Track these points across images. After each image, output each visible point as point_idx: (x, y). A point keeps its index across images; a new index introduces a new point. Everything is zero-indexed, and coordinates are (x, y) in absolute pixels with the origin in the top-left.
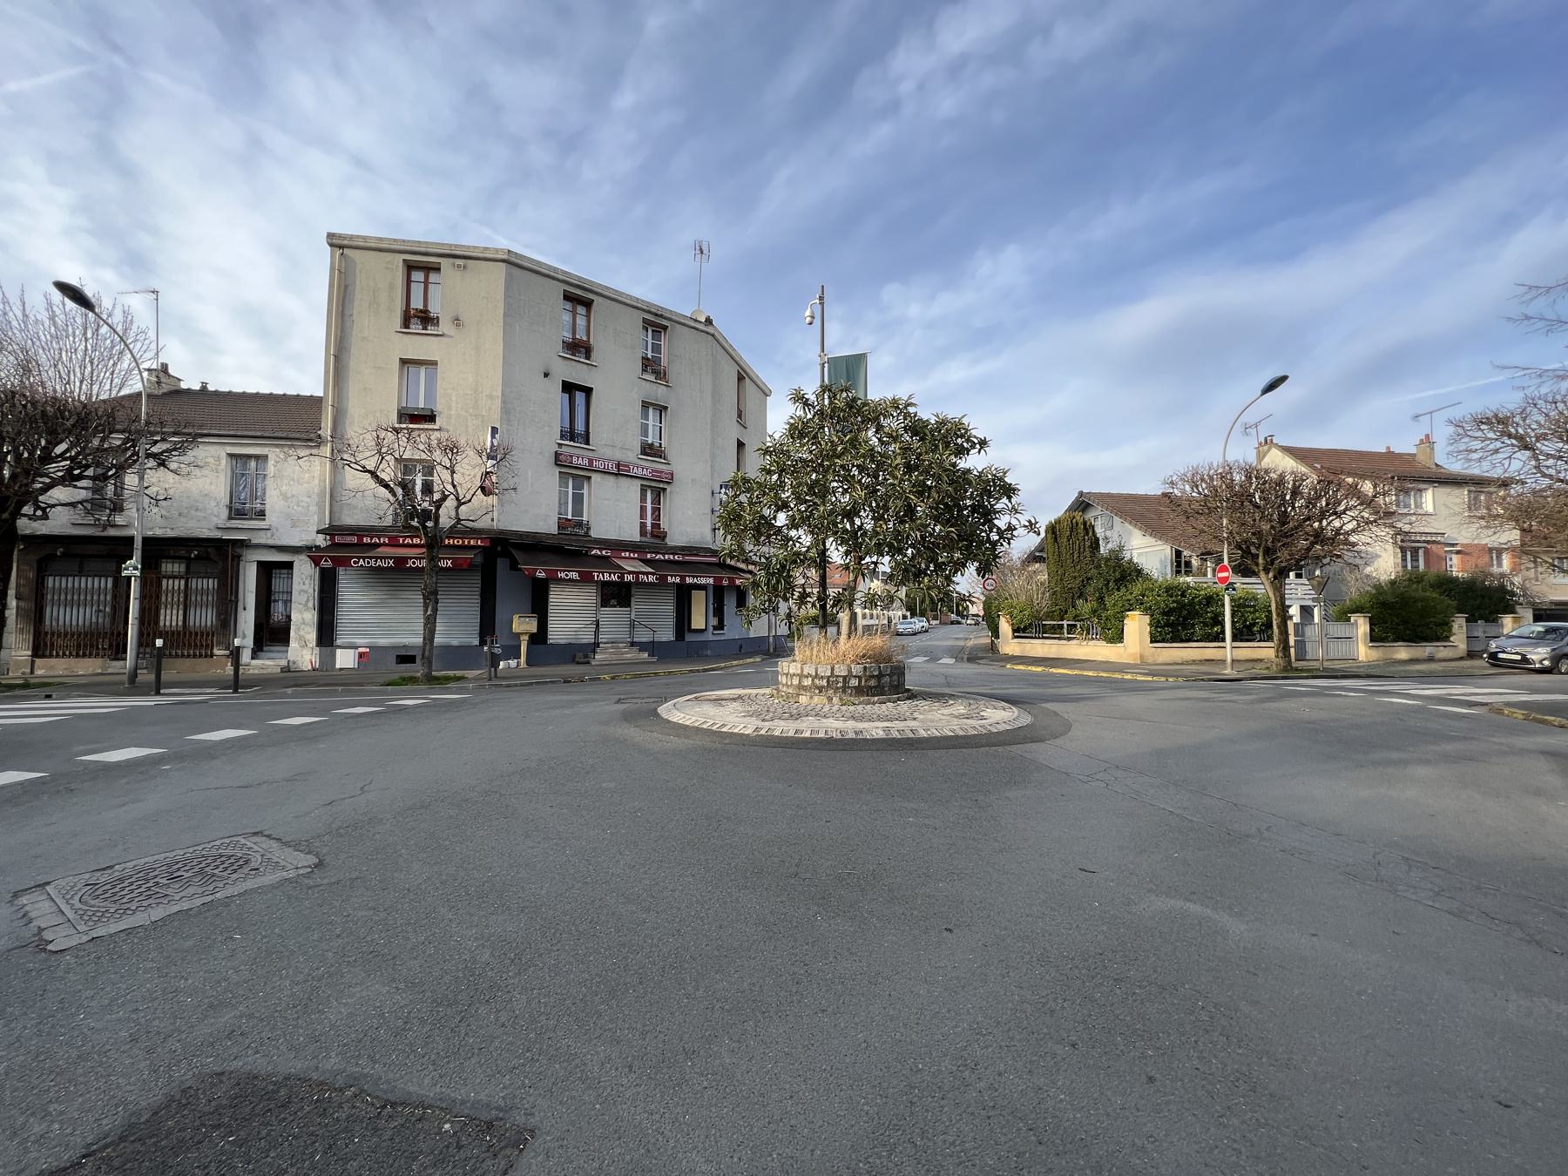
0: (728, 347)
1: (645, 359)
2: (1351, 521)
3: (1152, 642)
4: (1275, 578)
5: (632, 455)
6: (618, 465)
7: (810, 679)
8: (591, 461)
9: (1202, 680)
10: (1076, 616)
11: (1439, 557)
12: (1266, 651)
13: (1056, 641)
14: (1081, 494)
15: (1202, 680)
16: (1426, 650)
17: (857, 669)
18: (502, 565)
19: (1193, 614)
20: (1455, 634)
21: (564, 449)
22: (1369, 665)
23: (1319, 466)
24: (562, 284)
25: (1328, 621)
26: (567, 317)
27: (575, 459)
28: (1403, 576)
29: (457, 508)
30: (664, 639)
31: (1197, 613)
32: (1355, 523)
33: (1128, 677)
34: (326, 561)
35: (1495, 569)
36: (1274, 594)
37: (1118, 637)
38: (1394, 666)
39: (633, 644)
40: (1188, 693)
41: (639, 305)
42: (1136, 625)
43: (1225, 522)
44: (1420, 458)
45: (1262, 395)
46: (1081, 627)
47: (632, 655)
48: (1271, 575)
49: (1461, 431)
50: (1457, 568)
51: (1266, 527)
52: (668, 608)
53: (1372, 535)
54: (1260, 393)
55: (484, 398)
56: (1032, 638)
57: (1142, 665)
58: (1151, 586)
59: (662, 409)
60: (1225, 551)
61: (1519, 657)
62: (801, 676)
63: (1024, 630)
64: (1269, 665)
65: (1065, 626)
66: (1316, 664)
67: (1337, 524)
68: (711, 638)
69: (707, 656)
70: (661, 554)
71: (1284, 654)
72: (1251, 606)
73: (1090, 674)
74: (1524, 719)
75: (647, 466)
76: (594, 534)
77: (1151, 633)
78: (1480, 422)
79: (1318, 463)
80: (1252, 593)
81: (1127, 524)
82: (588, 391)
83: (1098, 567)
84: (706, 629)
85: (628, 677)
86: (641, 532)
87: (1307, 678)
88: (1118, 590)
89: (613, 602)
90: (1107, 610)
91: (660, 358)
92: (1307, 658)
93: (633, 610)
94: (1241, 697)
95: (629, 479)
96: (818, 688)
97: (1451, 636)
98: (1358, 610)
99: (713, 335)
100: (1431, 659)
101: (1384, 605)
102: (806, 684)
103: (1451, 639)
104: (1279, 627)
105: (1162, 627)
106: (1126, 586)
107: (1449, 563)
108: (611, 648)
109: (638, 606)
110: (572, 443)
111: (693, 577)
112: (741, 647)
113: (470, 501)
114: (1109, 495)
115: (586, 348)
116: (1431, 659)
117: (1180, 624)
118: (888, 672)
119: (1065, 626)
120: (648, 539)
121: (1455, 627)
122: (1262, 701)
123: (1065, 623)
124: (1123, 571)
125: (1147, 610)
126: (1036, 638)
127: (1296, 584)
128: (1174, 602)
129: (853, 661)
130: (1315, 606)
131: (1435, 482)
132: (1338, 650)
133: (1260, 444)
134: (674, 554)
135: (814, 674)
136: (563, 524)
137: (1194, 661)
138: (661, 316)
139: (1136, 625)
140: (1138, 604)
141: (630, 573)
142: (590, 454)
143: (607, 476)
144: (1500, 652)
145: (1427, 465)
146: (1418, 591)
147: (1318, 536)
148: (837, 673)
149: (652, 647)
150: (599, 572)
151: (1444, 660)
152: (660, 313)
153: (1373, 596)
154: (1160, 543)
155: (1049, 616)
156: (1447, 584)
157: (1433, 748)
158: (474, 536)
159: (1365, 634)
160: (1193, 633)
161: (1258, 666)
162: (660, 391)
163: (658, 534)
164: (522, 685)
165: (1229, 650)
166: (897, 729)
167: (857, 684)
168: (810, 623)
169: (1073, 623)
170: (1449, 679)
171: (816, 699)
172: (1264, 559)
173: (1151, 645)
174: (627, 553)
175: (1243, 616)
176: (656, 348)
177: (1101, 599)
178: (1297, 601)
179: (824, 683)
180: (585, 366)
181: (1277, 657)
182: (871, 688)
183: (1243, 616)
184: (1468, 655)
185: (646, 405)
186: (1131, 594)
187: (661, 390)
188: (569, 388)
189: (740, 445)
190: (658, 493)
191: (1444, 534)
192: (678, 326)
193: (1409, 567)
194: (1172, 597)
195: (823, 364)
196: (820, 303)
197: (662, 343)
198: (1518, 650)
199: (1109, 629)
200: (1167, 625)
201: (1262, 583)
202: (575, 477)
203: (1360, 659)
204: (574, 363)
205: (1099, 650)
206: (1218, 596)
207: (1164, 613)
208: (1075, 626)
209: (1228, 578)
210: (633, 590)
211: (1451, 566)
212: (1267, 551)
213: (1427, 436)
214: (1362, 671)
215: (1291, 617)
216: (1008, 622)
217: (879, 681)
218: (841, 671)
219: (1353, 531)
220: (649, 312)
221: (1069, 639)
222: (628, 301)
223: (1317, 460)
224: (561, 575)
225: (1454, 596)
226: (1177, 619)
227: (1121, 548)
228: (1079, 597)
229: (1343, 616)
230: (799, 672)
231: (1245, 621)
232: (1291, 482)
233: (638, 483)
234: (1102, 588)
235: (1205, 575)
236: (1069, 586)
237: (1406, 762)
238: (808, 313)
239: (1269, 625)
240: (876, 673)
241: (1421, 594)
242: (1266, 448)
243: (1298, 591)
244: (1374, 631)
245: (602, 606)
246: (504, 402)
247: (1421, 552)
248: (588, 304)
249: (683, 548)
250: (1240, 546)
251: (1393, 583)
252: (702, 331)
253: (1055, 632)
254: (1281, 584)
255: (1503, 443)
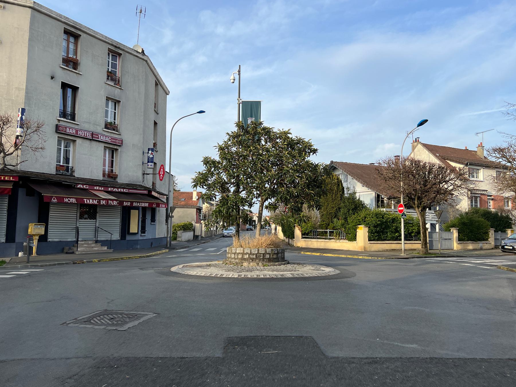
0: (152, 68)
1: (108, 72)
2: (451, 185)
3: (369, 240)
4: (422, 211)
5: (100, 129)
6: (92, 134)
7: (248, 255)
8: (77, 131)
9: (393, 258)
10: (334, 227)
11: (485, 201)
12: (417, 245)
13: (324, 240)
14: (332, 162)
15: (393, 258)
16: (480, 245)
17: (269, 250)
18: (21, 193)
19: (387, 227)
20: (490, 238)
21: (61, 123)
22: (458, 251)
23: (438, 155)
24: (64, 25)
25: (442, 231)
26: (64, 44)
27: (68, 130)
28: (471, 210)
29: (4, 158)
30: (69, 240)
31: (389, 227)
32: (452, 186)
33: (361, 257)
34: (54, 199)
35: (506, 208)
36: (421, 218)
37: (353, 238)
38: (467, 252)
39: (97, 242)
40: (391, 262)
41: (107, 41)
42: (362, 232)
43: (402, 183)
44: (479, 153)
45: (418, 127)
46: (336, 233)
47: (97, 248)
48: (420, 209)
49: (488, 153)
50: (492, 207)
51: (418, 187)
52: (117, 221)
53: (459, 192)
54: (417, 126)
55: (14, 90)
56: (311, 238)
57: (365, 252)
58: (369, 213)
59: (116, 102)
60: (402, 197)
61: (511, 248)
62: (243, 254)
63: (307, 234)
64: (419, 252)
65: (328, 232)
66: (438, 251)
67: (446, 186)
68: (141, 238)
69: (137, 249)
70: (122, 188)
71: (425, 246)
72: (411, 224)
73: (343, 256)
74: (507, 270)
75: (107, 136)
76: (77, 175)
77: (369, 236)
78: (495, 150)
79: (438, 153)
80: (412, 217)
81: (355, 180)
82: (75, 89)
83: (344, 202)
84: (138, 233)
85: (107, 260)
86: (103, 174)
87: (434, 257)
88: (354, 214)
89: (86, 216)
90: (349, 224)
91: (116, 71)
92: (434, 248)
93: (98, 221)
94: (412, 264)
95: (98, 143)
96: (251, 259)
97: (489, 238)
98: (453, 226)
99: (146, 61)
100: (481, 249)
101: (464, 224)
102: (245, 257)
103: (489, 240)
104: (423, 234)
105: (373, 233)
106: (357, 212)
107: (489, 204)
108: (85, 244)
109: (100, 220)
110: (65, 120)
111: (138, 202)
112: (152, 244)
113: (12, 153)
114: (346, 164)
115: (74, 63)
116: (481, 249)
117: (381, 232)
118: (280, 252)
119: (328, 232)
120: (106, 178)
121: (490, 234)
122: (419, 265)
123: (328, 230)
124: (356, 205)
125: (367, 225)
126: (313, 238)
127: (429, 213)
128: (379, 221)
129: (266, 247)
130: (437, 224)
131: (484, 166)
132: (446, 245)
133: (414, 141)
134: (124, 188)
135: (250, 252)
136: (59, 168)
137: (387, 250)
138: (119, 48)
139: (362, 232)
140: (363, 221)
141: (104, 199)
142: (76, 127)
143: (85, 141)
144: (505, 245)
145: (481, 157)
146: (476, 218)
147: (438, 192)
148: (260, 252)
149: (109, 244)
150: (87, 199)
151: (486, 250)
152: (118, 46)
153: (460, 220)
154: (370, 190)
155: (321, 227)
156: (487, 215)
157: (476, 277)
158: (9, 174)
159: (456, 237)
160: (387, 237)
161: (415, 252)
162: (116, 92)
163: (112, 176)
164: (50, 265)
165: (403, 245)
166: (296, 274)
167: (269, 257)
168: (181, 229)
169: (332, 231)
170: (487, 257)
171: (251, 264)
172: (417, 202)
173: (369, 242)
174: (98, 187)
175: (408, 228)
176: (114, 66)
177: (346, 219)
178: (429, 221)
179: (254, 256)
180: (75, 74)
181: (422, 247)
182: (274, 258)
183: (408, 228)
184: (495, 247)
185: (108, 99)
186: (360, 216)
187: (117, 91)
188: (65, 86)
189: (155, 123)
190: (113, 152)
191: (487, 191)
192: (127, 54)
193: (474, 206)
194: (378, 218)
195: (240, 104)
196: (239, 74)
197: (117, 63)
198: (511, 244)
199: (350, 234)
200: (376, 232)
201: (416, 212)
202: (65, 139)
203: (454, 249)
204: (68, 72)
205: (344, 244)
206: (397, 218)
207: (375, 227)
208: (333, 232)
209: (403, 210)
210: (98, 210)
211: (490, 206)
212: (419, 198)
213: (481, 143)
214: (455, 254)
215: (427, 229)
216: (299, 230)
217: (277, 256)
218: (262, 251)
219: (452, 190)
220: (112, 45)
221: (330, 239)
222: (101, 38)
223: (437, 152)
224: (66, 200)
225: (490, 220)
226: (380, 229)
227: (355, 193)
228: (335, 217)
229: (447, 229)
230: (242, 252)
231: (409, 231)
232: (428, 167)
233: (103, 145)
234: (346, 213)
235: (391, 208)
236: (330, 212)
237: (467, 281)
238: (232, 77)
239: (419, 233)
240: (276, 252)
241: (477, 219)
242: (416, 144)
243: (430, 216)
244: (460, 236)
245: (80, 218)
246: (27, 93)
247: (478, 199)
248: (76, 37)
249: (128, 185)
250: (408, 195)
251: (467, 213)
252: (140, 58)
253: (323, 235)
254: (424, 214)
255: (502, 159)
